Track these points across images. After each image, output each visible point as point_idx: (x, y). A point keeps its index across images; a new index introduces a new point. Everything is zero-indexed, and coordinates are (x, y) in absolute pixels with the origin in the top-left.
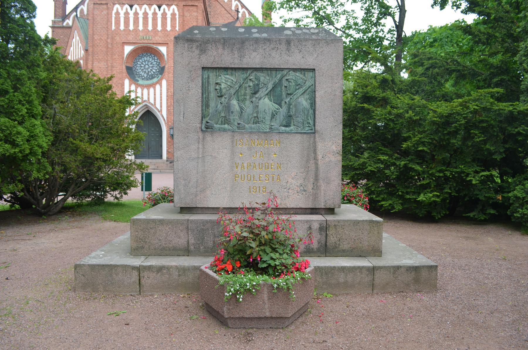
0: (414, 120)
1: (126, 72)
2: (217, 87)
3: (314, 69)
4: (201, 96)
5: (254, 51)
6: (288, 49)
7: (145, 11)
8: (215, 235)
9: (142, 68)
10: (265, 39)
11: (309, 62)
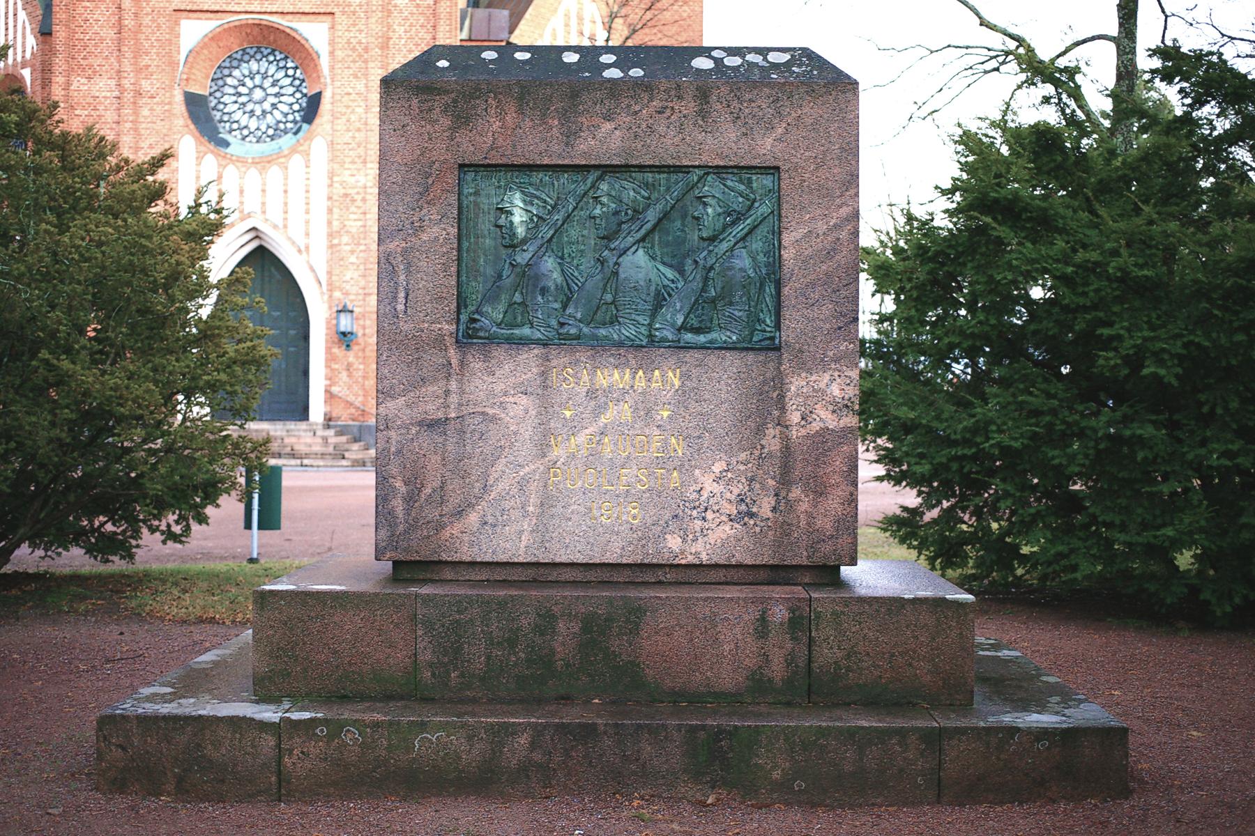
0: (76, 541)
1: (186, 114)
2: (502, 222)
3: (777, 168)
4: (455, 246)
5: (608, 118)
6: (701, 110)
8: (492, 639)
9: (243, 99)
10: (637, 82)
11: (766, 147)
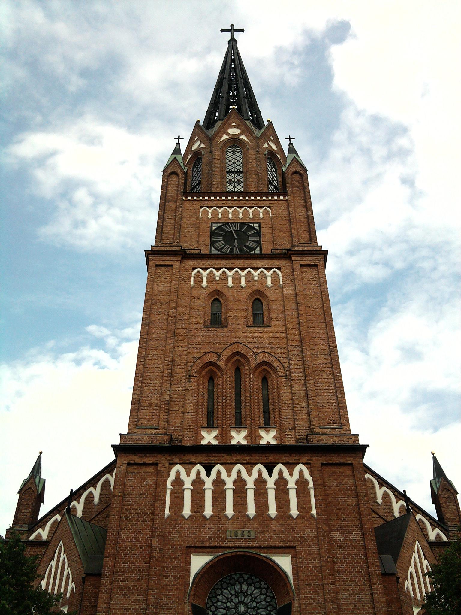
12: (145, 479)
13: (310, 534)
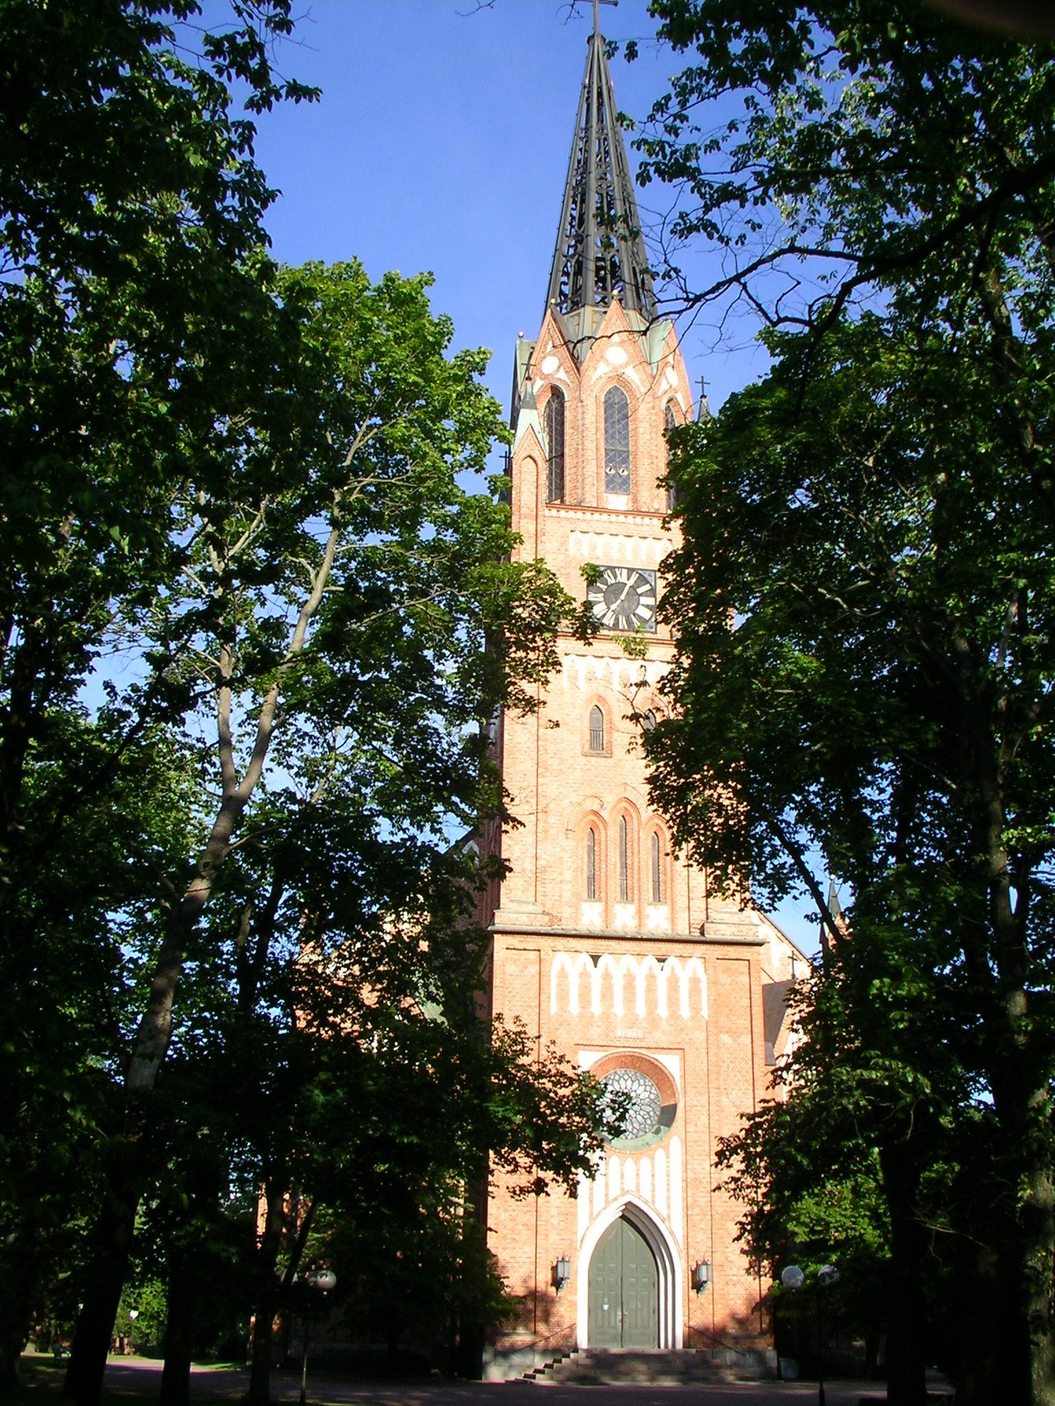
7: (673, 973)
12: (526, 967)
13: (700, 1036)
